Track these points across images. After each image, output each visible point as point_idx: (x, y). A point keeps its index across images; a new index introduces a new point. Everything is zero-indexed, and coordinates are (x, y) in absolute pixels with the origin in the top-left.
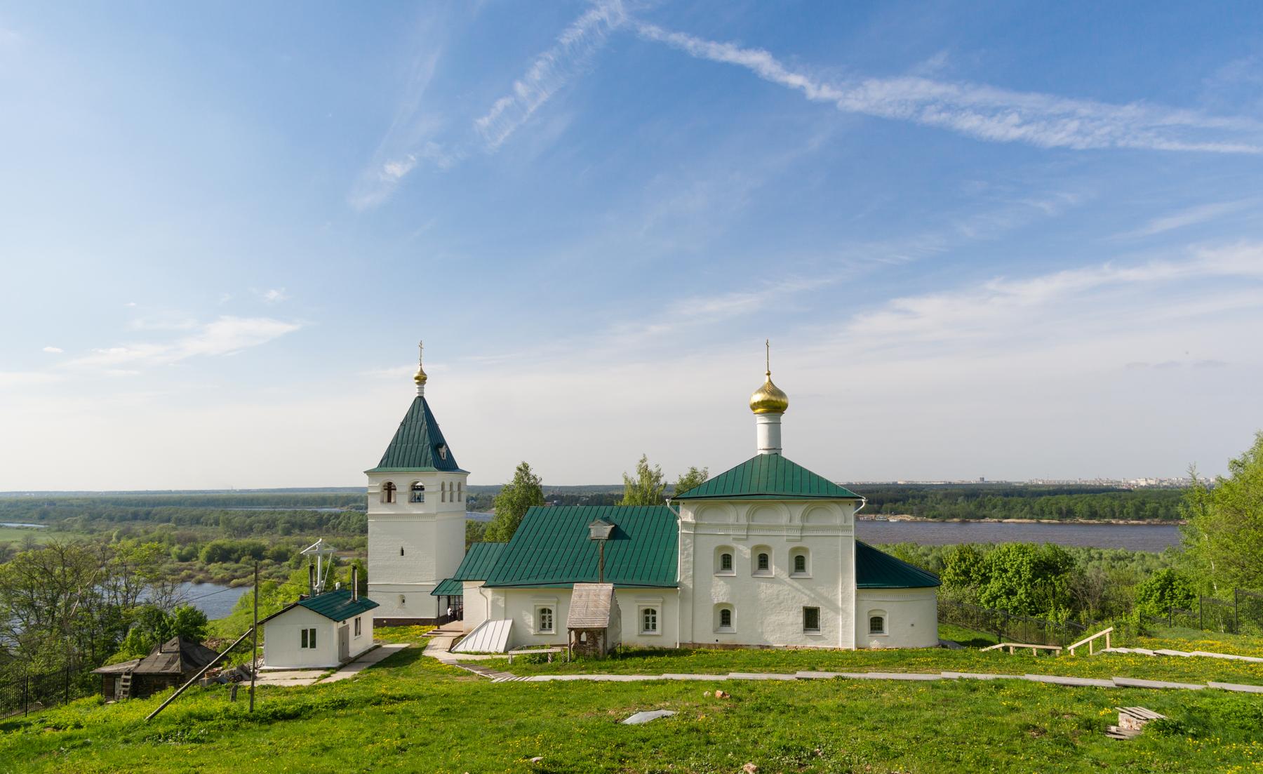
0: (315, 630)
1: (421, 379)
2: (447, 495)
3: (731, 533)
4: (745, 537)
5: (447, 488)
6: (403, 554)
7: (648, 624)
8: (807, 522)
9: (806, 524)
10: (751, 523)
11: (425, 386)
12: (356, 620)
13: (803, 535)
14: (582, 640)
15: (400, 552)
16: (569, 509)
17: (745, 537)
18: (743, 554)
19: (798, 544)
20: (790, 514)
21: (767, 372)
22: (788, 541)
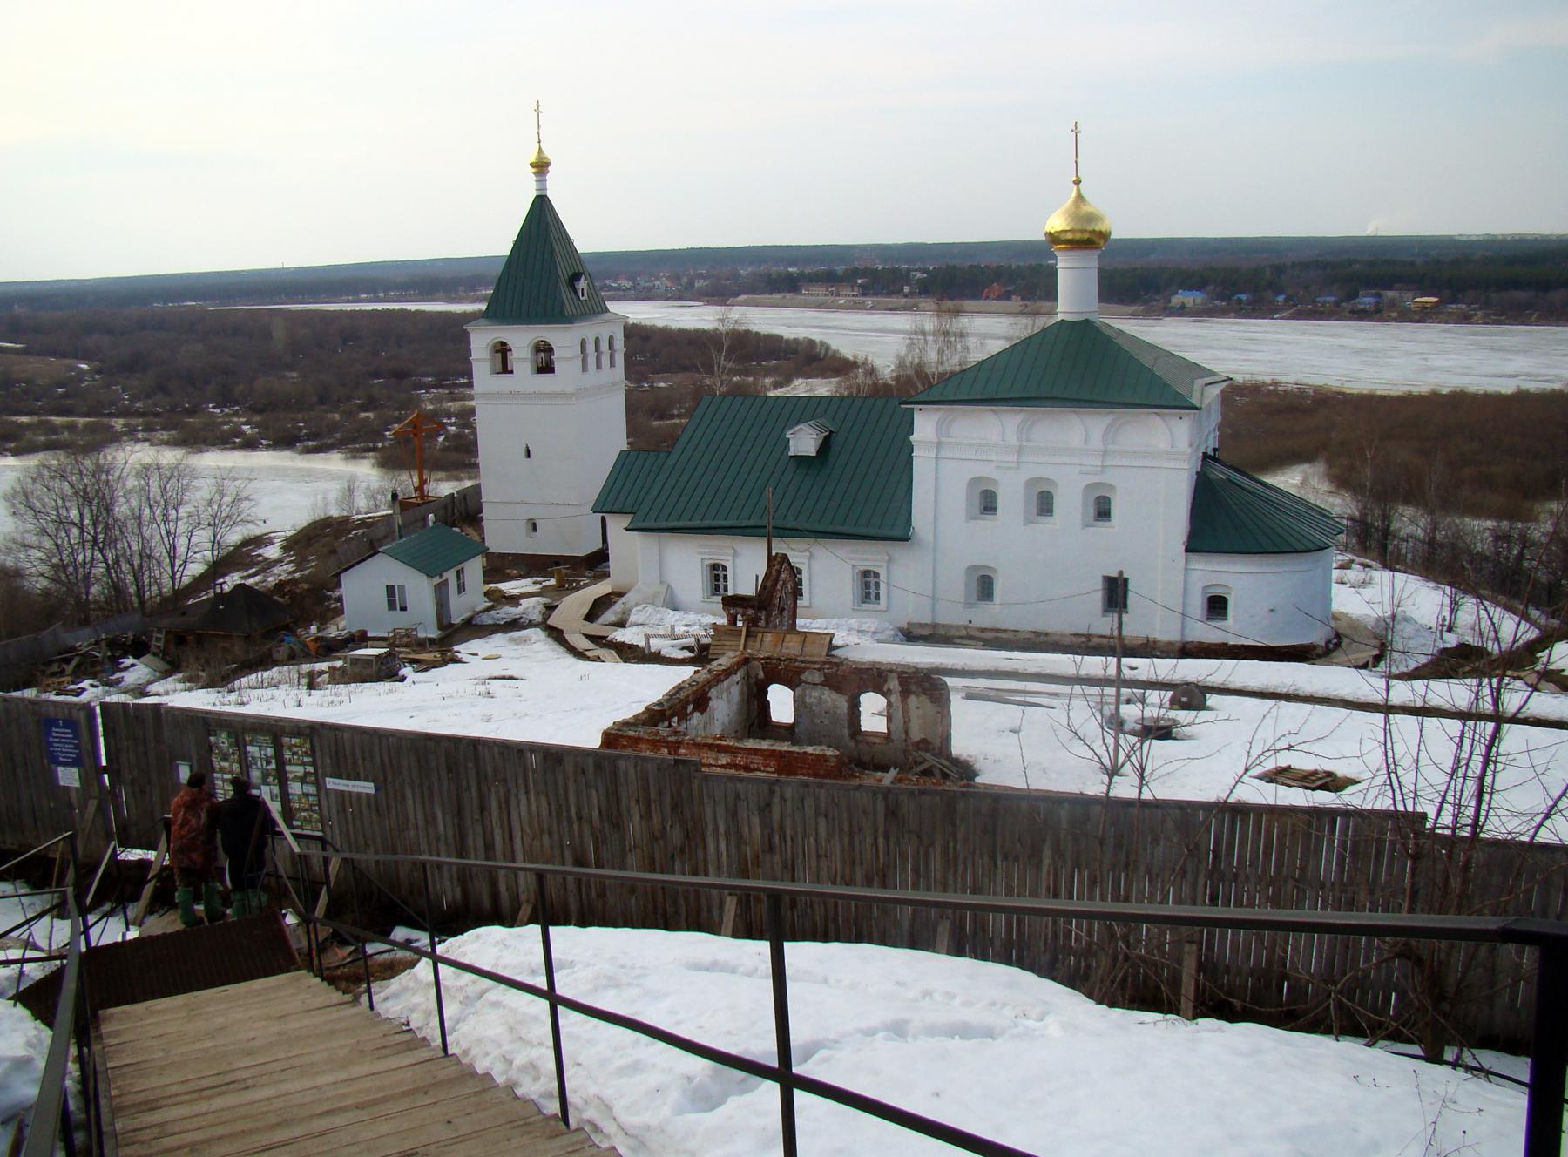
0: (389, 610)
1: (541, 167)
2: (591, 360)
3: (993, 457)
4: (1014, 465)
5: (591, 348)
6: (529, 456)
7: (869, 593)
8: (1113, 443)
9: (1111, 447)
10: (1025, 443)
11: (548, 177)
12: (458, 572)
13: (1107, 463)
14: (812, 452)
15: (523, 453)
16: (538, 844)
17: (1014, 465)
18: (1012, 499)
19: (1096, 479)
20: (1086, 431)
21: (1074, 179)
22: (1081, 473)
